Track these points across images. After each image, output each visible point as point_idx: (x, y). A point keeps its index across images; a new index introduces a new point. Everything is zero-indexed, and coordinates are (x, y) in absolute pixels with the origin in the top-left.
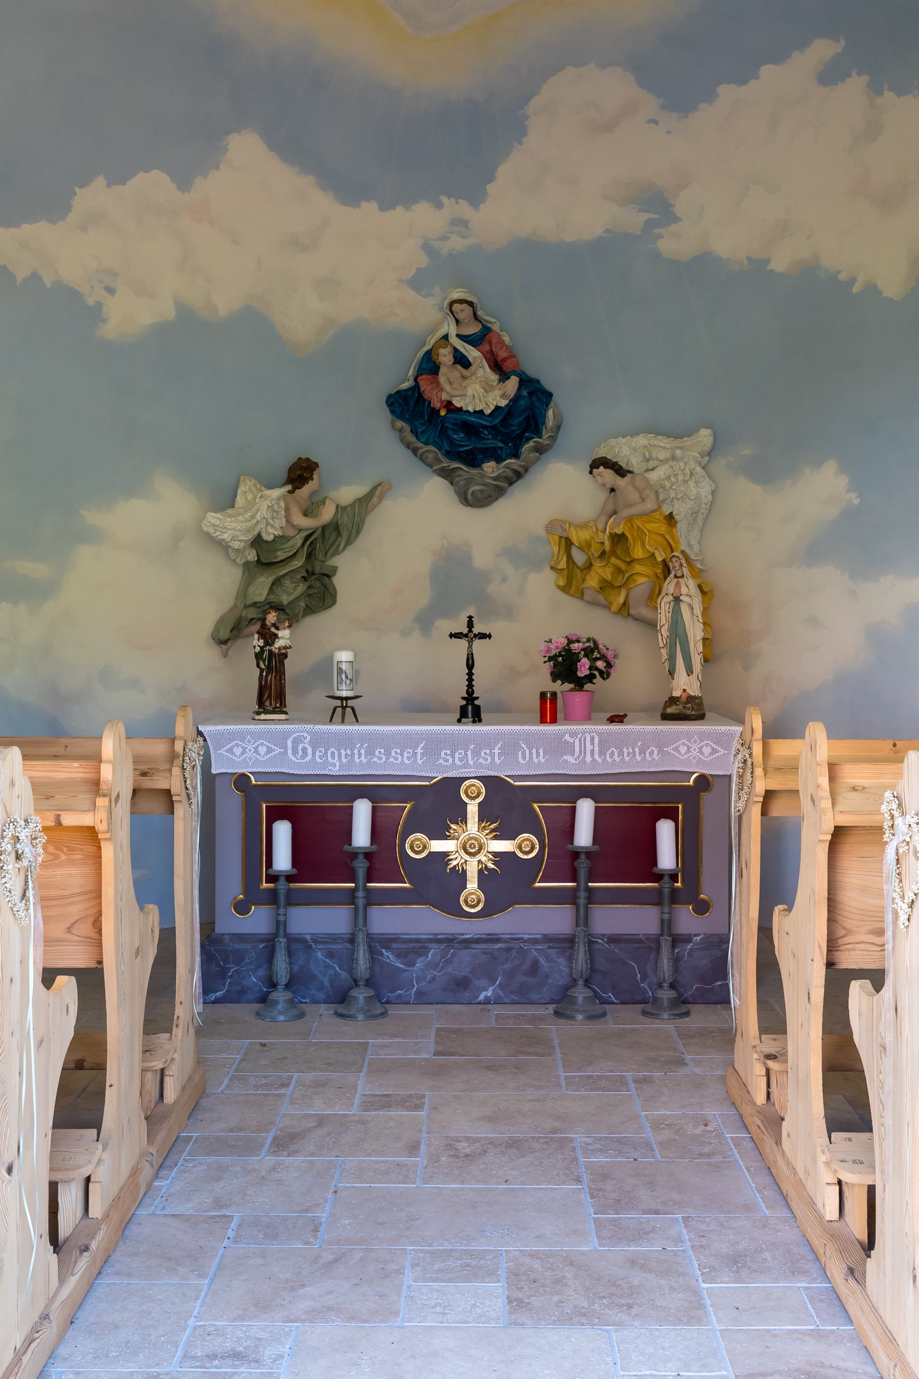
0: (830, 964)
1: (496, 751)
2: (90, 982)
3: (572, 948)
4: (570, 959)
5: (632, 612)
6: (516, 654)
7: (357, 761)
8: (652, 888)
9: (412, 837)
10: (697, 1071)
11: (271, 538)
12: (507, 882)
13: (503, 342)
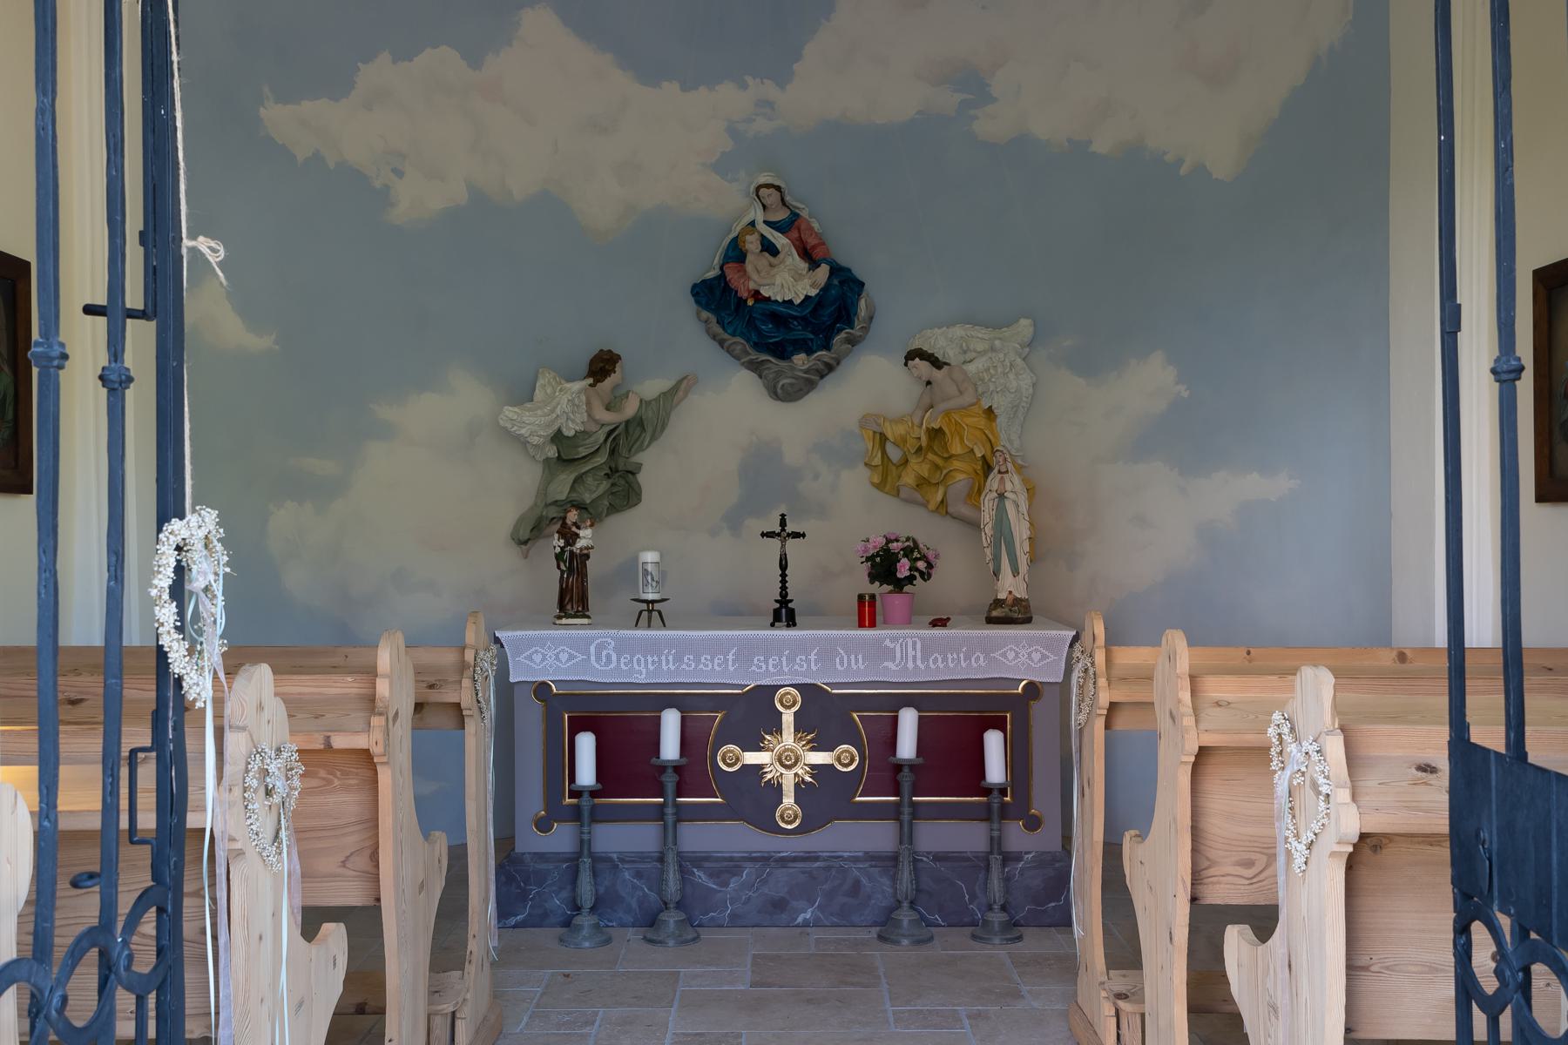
0: (1194, 899)
1: (813, 657)
2: (363, 923)
3: (896, 866)
4: (894, 879)
5: (951, 510)
6: (832, 554)
8: (979, 803)
10: (1035, 1004)
11: (571, 433)
12: (824, 795)
13: (811, 229)
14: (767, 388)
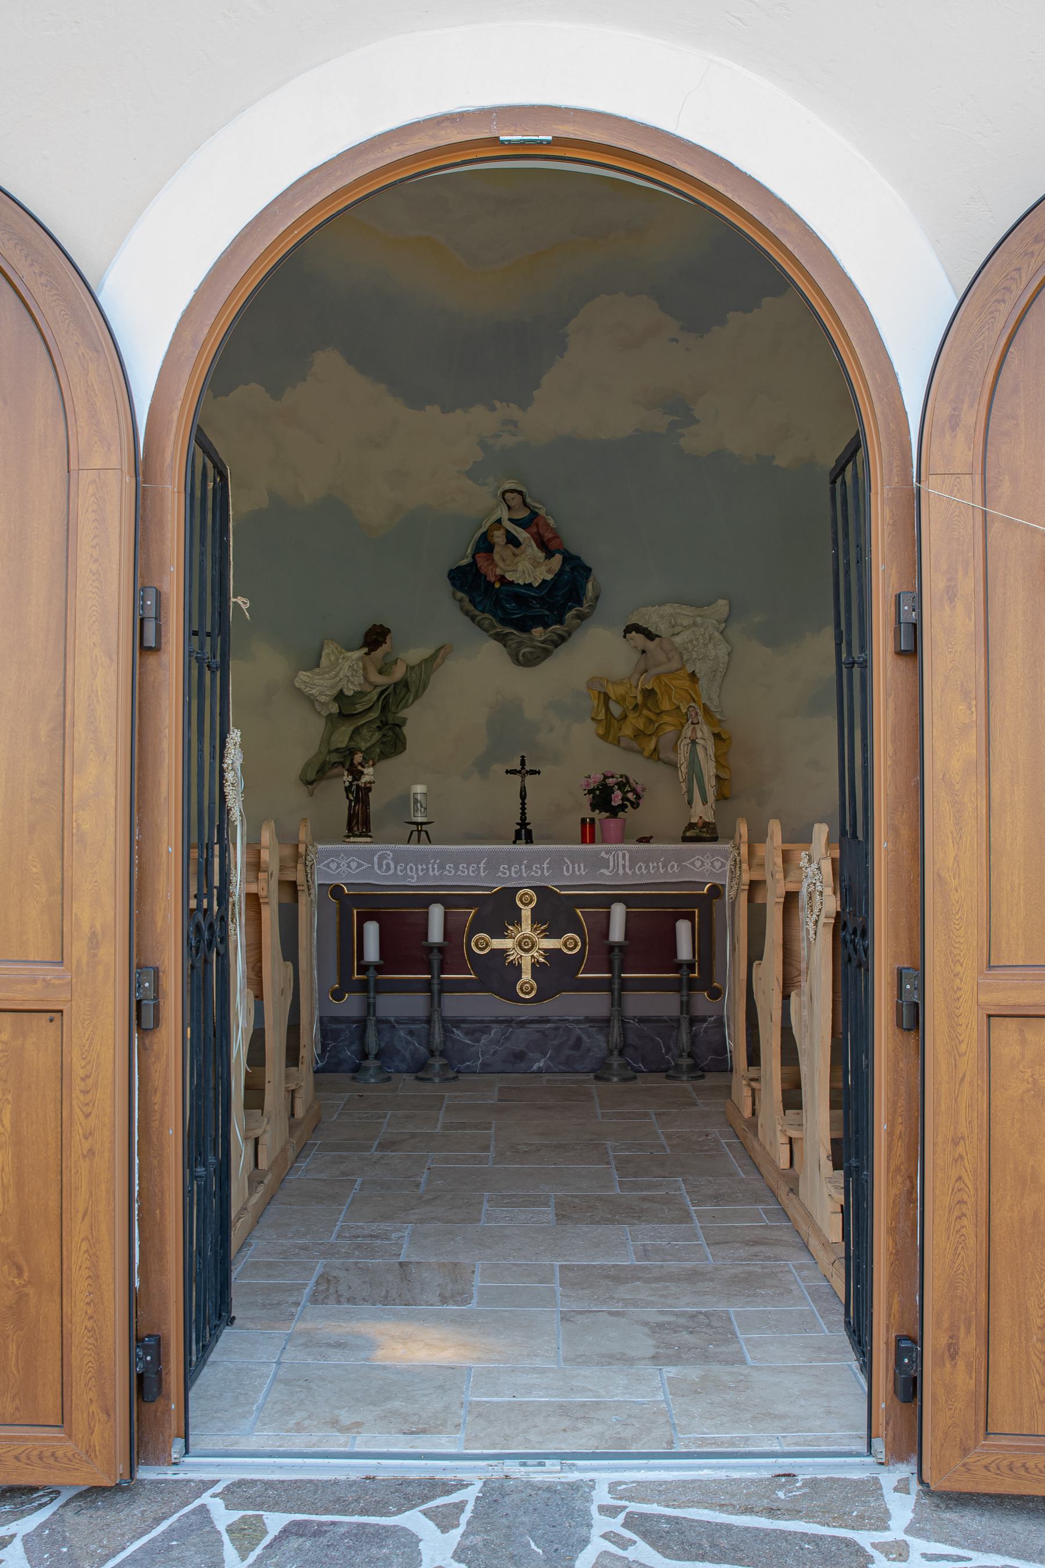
1: (545, 866)
4: (607, 1036)
5: (662, 756)
6: (559, 791)
7: (431, 874)
9: (477, 936)
11: (350, 693)
12: (555, 973)
13: (548, 525)
14: (510, 654)
